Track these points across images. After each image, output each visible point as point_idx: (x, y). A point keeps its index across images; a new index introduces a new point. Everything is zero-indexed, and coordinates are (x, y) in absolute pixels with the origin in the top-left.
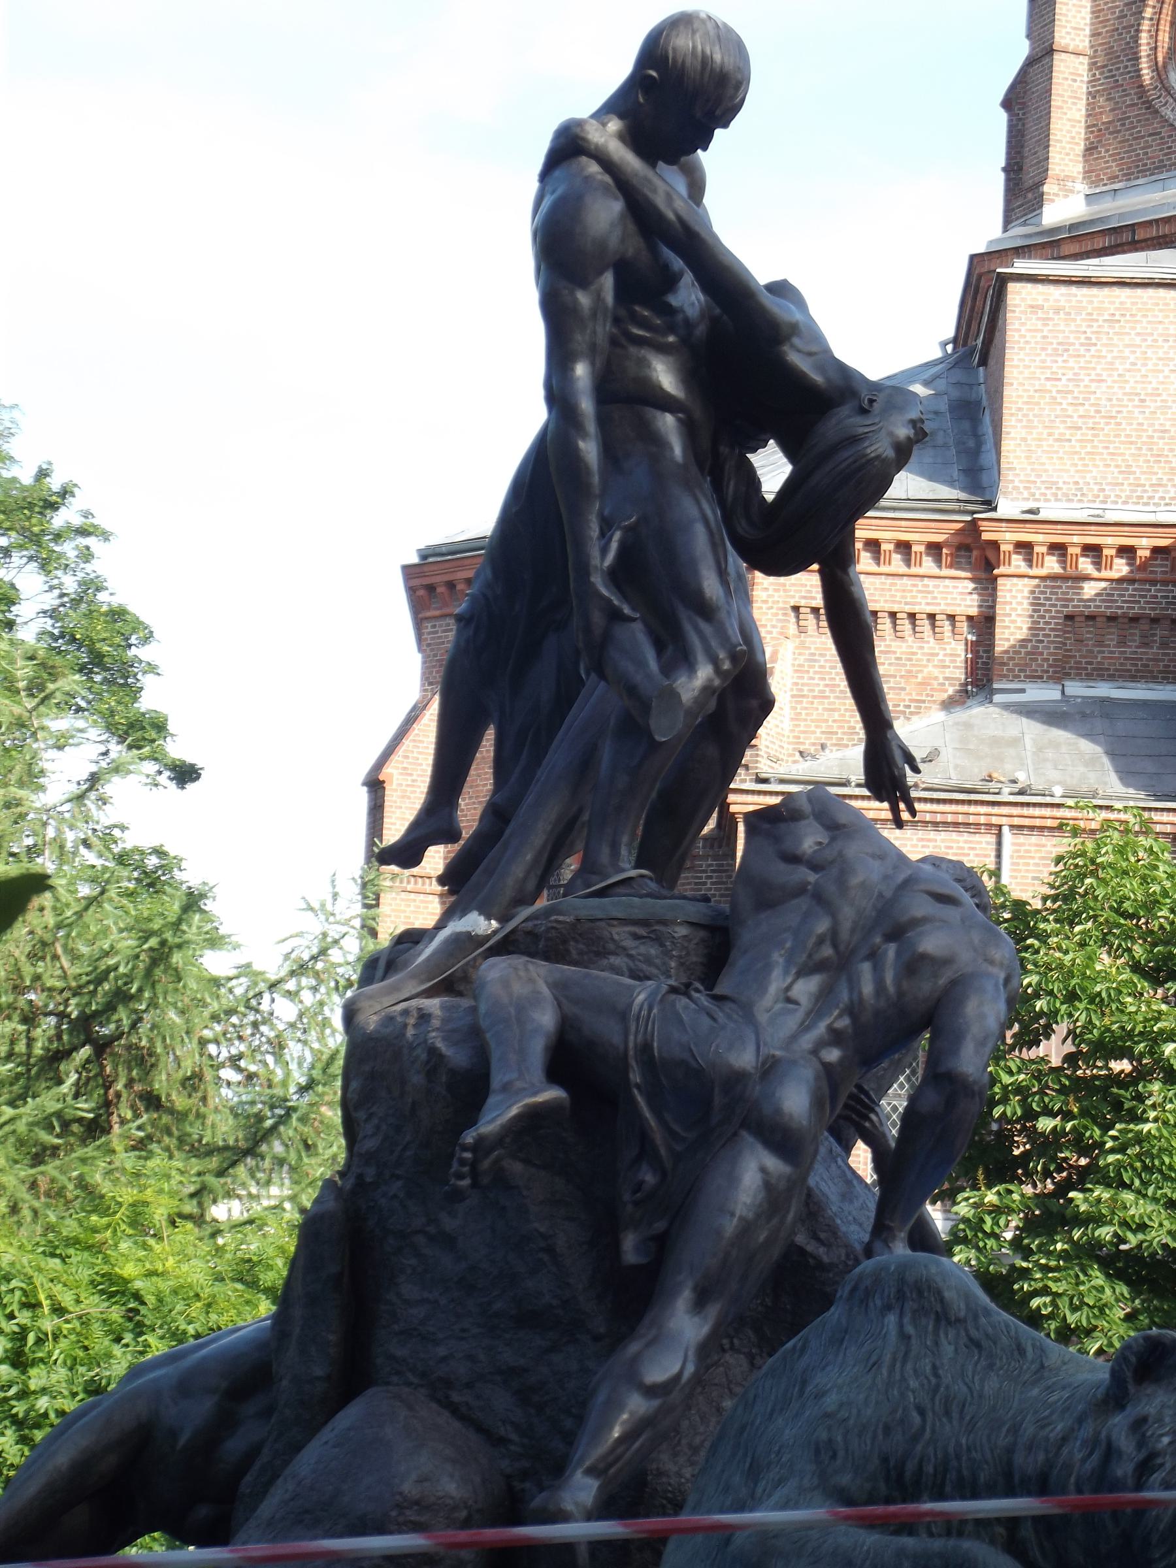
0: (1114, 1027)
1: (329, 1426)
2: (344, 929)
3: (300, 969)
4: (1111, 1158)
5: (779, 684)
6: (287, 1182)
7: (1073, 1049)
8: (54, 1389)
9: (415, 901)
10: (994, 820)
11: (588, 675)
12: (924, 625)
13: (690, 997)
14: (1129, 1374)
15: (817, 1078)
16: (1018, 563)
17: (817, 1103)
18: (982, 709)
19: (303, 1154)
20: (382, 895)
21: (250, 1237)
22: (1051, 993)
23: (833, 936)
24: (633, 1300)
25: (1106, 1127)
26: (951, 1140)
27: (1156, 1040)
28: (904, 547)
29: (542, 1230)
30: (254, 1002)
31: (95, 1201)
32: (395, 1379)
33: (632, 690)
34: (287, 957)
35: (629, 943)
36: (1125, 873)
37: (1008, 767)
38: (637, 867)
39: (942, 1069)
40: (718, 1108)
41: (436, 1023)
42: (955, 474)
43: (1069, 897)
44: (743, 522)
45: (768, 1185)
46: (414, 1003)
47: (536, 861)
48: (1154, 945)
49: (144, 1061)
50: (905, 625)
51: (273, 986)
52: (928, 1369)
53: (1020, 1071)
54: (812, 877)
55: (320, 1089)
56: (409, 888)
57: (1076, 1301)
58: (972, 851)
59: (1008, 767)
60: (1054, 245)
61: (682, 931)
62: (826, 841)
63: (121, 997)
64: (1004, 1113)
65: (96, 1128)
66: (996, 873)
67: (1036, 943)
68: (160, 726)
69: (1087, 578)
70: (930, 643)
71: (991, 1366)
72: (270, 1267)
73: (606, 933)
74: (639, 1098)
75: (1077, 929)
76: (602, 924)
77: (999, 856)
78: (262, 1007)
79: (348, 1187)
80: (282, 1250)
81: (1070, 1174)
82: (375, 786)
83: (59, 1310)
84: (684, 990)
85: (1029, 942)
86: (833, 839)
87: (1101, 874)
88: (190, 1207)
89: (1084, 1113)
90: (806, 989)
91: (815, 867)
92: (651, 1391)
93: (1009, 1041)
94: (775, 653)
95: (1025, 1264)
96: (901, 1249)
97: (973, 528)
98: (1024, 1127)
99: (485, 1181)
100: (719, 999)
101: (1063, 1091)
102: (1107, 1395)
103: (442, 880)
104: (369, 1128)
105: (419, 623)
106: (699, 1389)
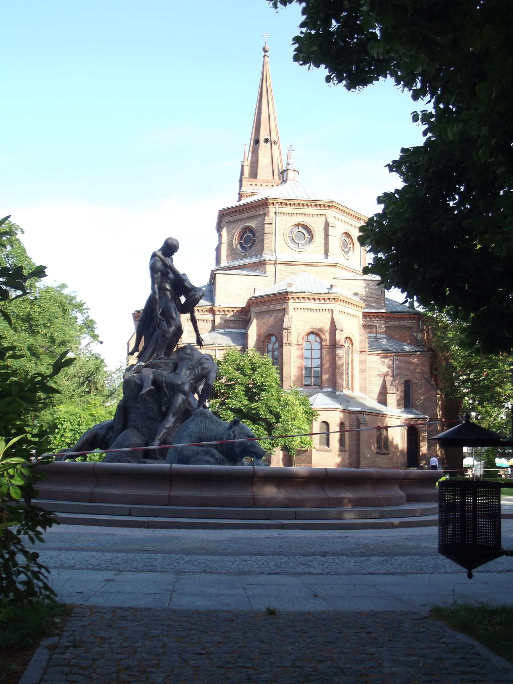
3: (117, 370)
8: (84, 429)
9: (134, 360)
16: (218, 313)
17: (190, 388)
23: (192, 365)
24: (164, 416)
26: (209, 393)
27: (237, 379)
31: (89, 403)
33: (163, 330)
43: (225, 359)
45: (183, 400)
49: (96, 383)
54: (189, 356)
58: (212, 353)
60: (222, 269)
61: (170, 364)
63: (92, 374)
65: (89, 393)
68: (98, 336)
82: (128, 344)
83: (84, 418)
88: (102, 404)
89: (227, 389)
90: (188, 372)
91: (189, 355)
92: (167, 428)
96: (201, 408)
100: (176, 374)
101: (225, 386)
103: (137, 357)
105: (134, 321)
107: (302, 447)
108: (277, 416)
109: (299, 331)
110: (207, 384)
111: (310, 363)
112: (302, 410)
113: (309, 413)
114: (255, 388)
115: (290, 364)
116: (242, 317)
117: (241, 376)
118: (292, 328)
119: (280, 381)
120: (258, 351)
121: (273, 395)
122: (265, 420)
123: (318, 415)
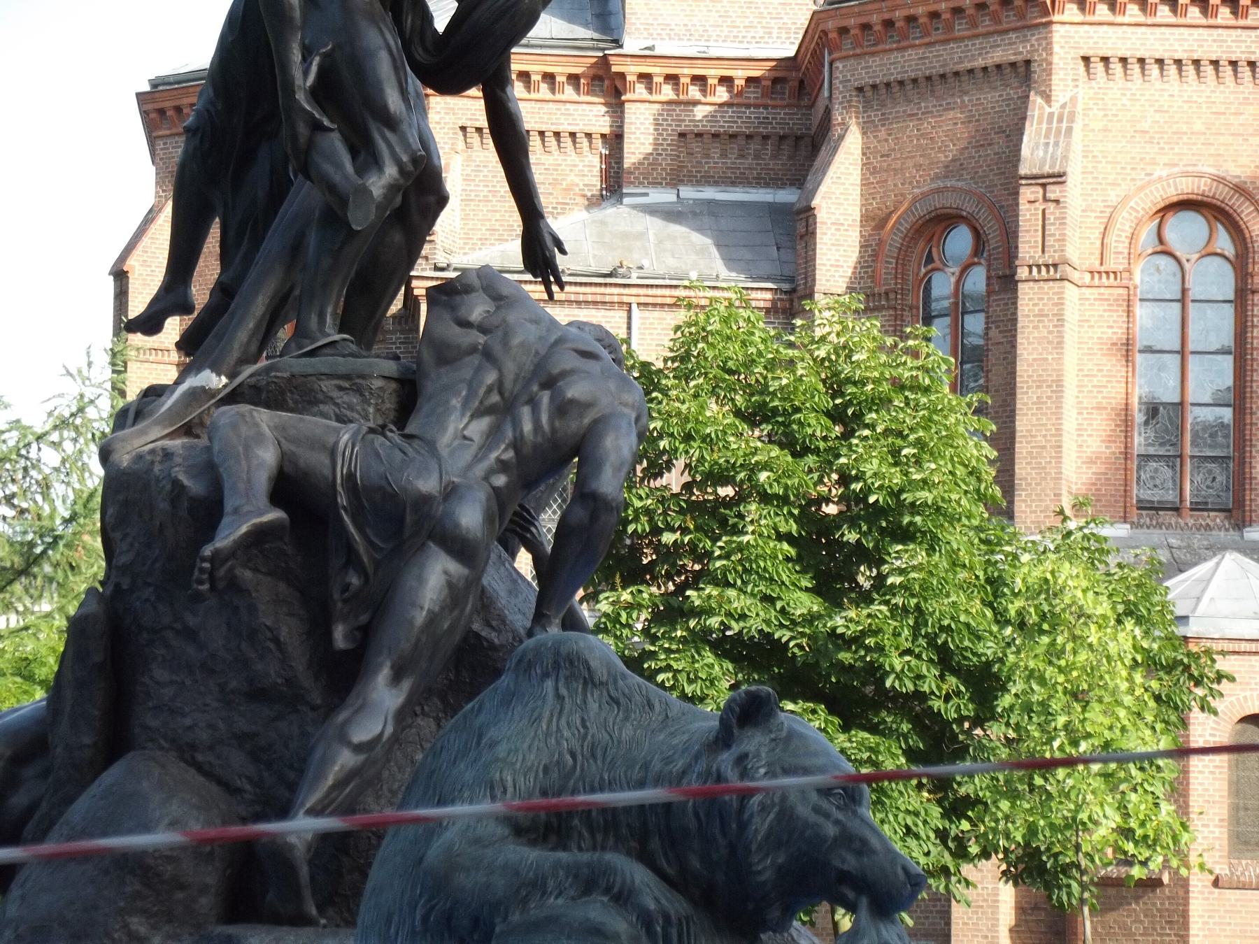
0: (721, 461)
1: (97, 782)
2: (99, 391)
4: (718, 564)
5: (453, 182)
6: (55, 595)
7: (690, 479)
9: (157, 361)
10: (626, 299)
11: (296, 177)
12: (567, 141)
13: (385, 437)
14: (734, 721)
15: (488, 500)
16: (641, 90)
17: (489, 519)
18: (614, 209)
19: (69, 573)
20: (129, 364)
21: (26, 641)
22: (672, 435)
23: (499, 386)
24: (343, 676)
25: (715, 540)
26: (595, 548)
27: (753, 470)
28: (549, 78)
29: (268, 624)
30: (23, 452)
32: (150, 744)
33: (331, 188)
34: (50, 414)
35: (336, 394)
36: (729, 338)
37: (636, 256)
38: (340, 332)
39: (586, 490)
40: (407, 524)
41: (178, 460)
42: (589, 18)
43: (684, 358)
44: (420, 50)
45: (450, 585)
46: (159, 443)
47: (257, 327)
48: (752, 395)
50: (551, 141)
51: (39, 438)
52: (578, 722)
53: (648, 496)
54: (482, 339)
55: (82, 521)
56: (151, 359)
57: (692, 676)
59: (636, 256)
61: (377, 383)
62: (492, 310)
64: (635, 530)
66: (628, 341)
67: (660, 396)
69: (696, 103)
70: (572, 156)
71: (626, 719)
72: (43, 664)
73: (316, 386)
74: (345, 517)
75: (692, 384)
76: (314, 379)
77: (629, 328)
78: (31, 456)
79: (108, 593)
80: (53, 650)
81: (687, 578)
82: (120, 275)
84: (381, 430)
85: (654, 395)
86: (498, 308)
87: (710, 339)
91: (483, 330)
92: (358, 748)
93: (639, 474)
94: (448, 164)
95: (652, 648)
96: (554, 630)
97: (604, 62)
98: (651, 542)
99: (221, 585)
101: (681, 512)
102: (717, 737)
104: (124, 546)
106: (396, 747)
107: (1129, 862)
108: (984, 683)
109: (1113, 196)
110: (586, 496)
111: (1173, 381)
112: (1128, 646)
113: (1170, 668)
114: (854, 524)
115: (1058, 387)
116: (782, 118)
117: (775, 451)
118: (1073, 179)
119: (997, 480)
120: (869, 311)
121: (955, 564)
122: (912, 705)
123: (1220, 677)
